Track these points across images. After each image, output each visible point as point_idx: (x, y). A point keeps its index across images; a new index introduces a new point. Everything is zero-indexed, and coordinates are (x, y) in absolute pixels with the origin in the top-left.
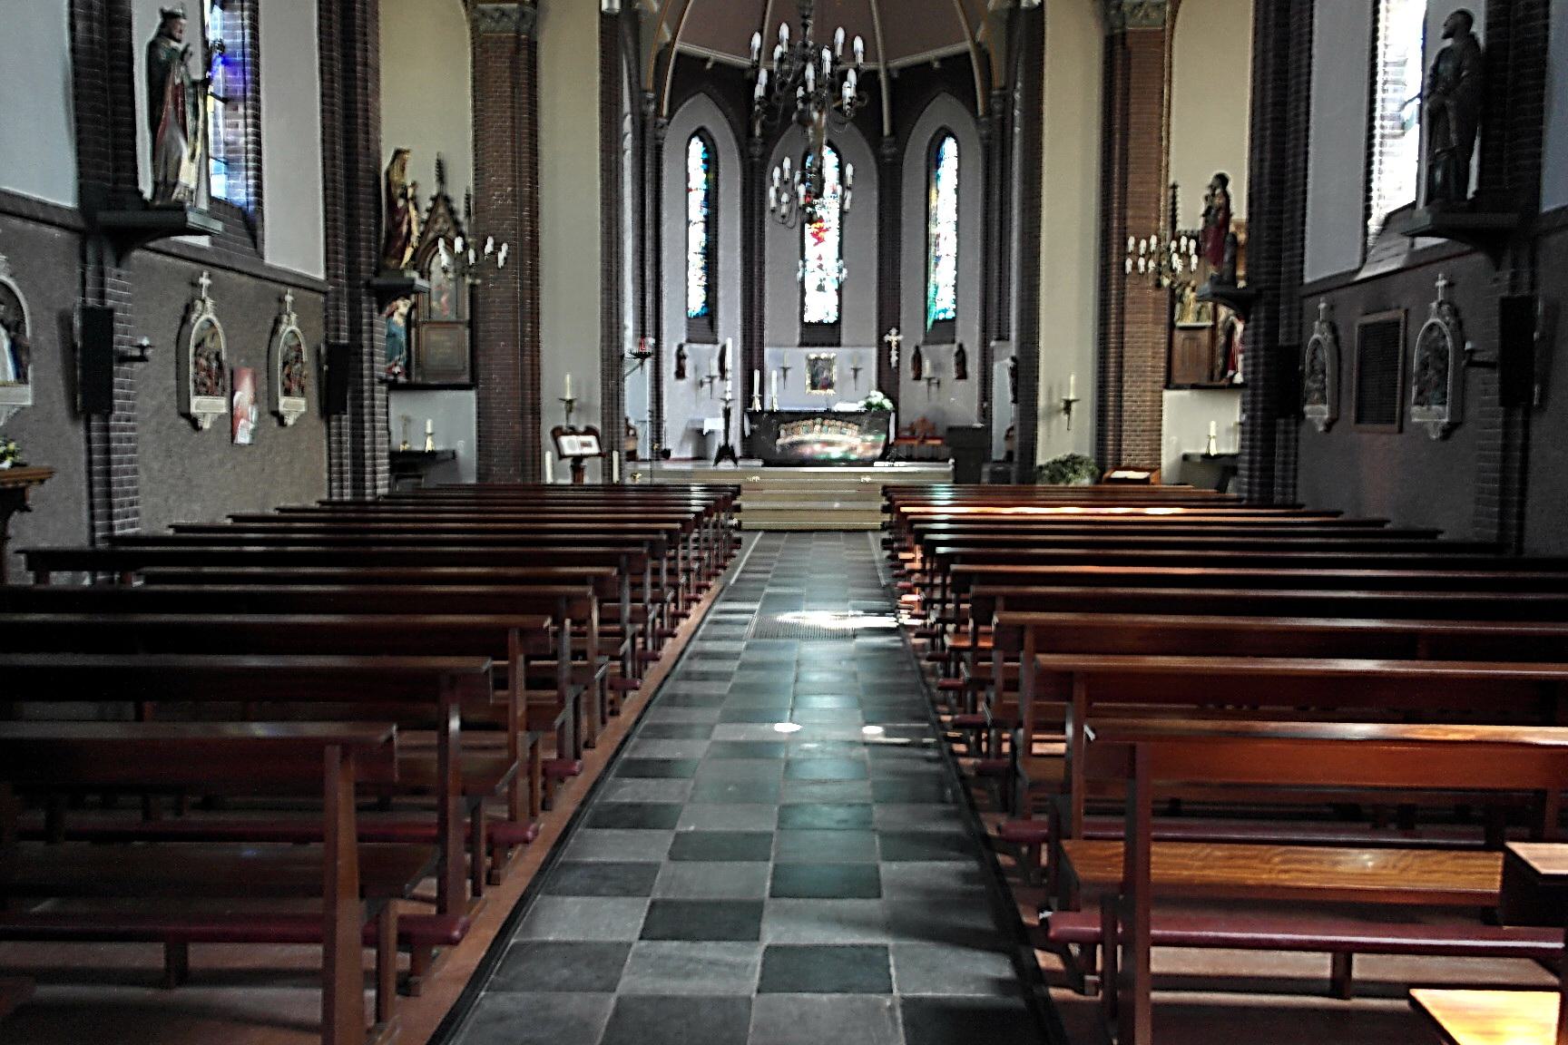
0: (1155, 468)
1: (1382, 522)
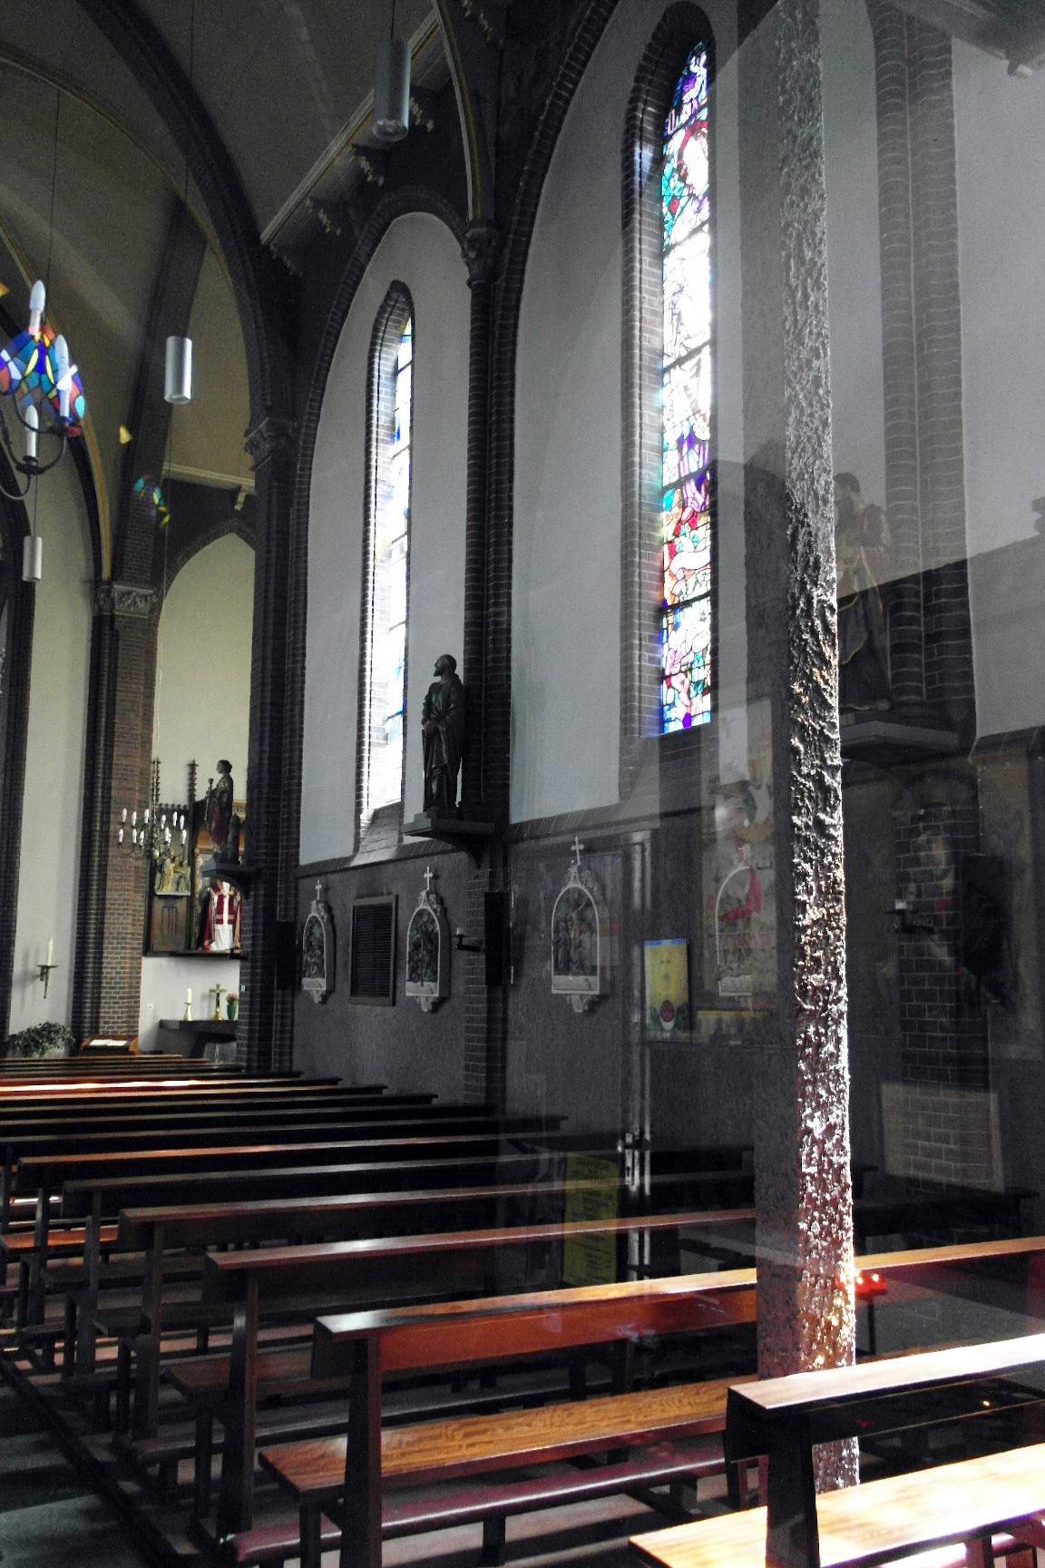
0: (132, 1037)
1: (379, 1089)
